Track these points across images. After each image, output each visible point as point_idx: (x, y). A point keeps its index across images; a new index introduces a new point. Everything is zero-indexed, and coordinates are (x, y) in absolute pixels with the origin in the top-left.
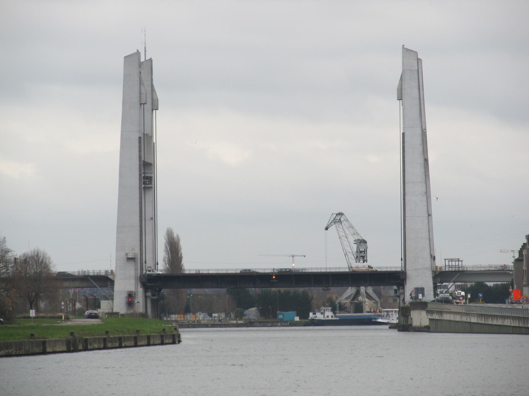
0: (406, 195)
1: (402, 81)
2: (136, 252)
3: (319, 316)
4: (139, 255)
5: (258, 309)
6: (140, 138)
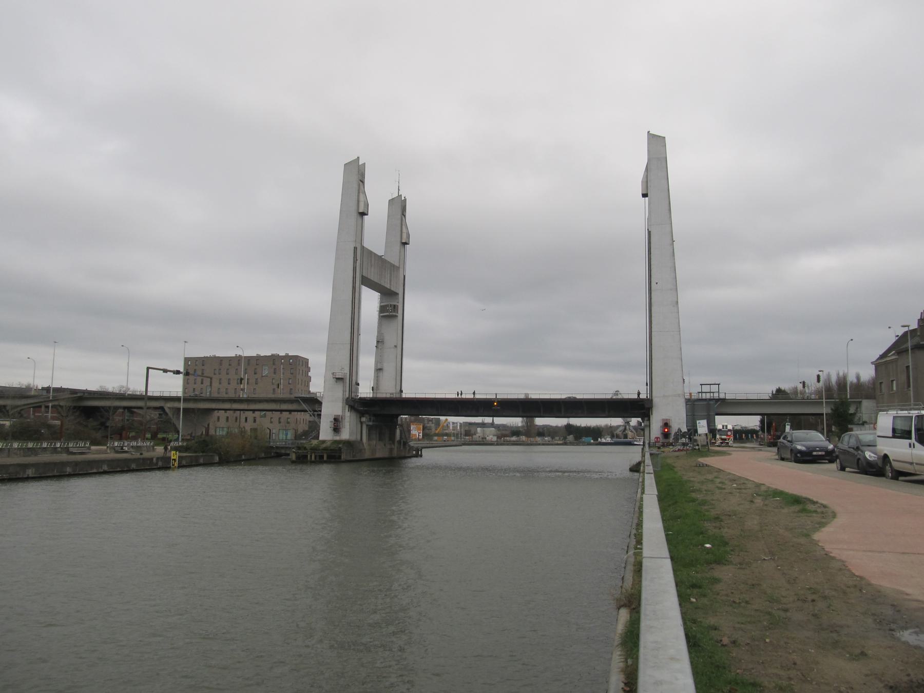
0: (652, 305)
2: (346, 372)
3: (603, 440)
4: (348, 375)
5: (574, 436)
6: (355, 248)
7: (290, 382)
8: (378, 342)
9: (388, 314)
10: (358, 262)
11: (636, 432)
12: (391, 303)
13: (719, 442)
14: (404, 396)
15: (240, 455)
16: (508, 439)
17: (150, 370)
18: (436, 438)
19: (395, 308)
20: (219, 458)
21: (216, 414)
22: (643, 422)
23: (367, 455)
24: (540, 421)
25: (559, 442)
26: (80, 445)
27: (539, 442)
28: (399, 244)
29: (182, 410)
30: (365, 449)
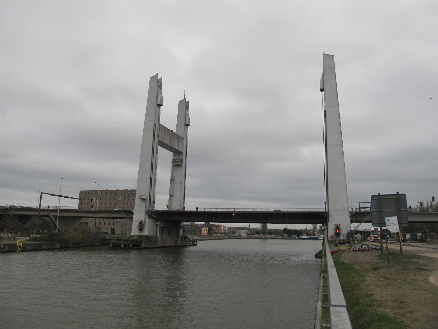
0: (328, 155)
1: (323, 76)
3: (303, 237)
6: (155, 124)
7: (132, 204)
8: (171, 180)
9: (176, 164)
10: (156, 132)
11: (320, 232)
12: (179, 158)
13: (373, 239)
14: (186, 210)
15: (80, 244)
16: (253, 235)
17: (42, 194)
18: (214, 235)
19: (181, 161)
20: (60, 245)
21: (83, 220)
22: (323, 226)
23: (160, 244)
24: (271, 226)
25: (279, 238)
26: (6, 235)
27: (269, 238)
28: (184, 125)
29: (58, 216)
30: (158, 241)
